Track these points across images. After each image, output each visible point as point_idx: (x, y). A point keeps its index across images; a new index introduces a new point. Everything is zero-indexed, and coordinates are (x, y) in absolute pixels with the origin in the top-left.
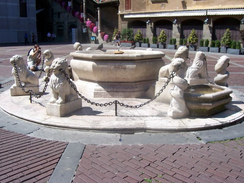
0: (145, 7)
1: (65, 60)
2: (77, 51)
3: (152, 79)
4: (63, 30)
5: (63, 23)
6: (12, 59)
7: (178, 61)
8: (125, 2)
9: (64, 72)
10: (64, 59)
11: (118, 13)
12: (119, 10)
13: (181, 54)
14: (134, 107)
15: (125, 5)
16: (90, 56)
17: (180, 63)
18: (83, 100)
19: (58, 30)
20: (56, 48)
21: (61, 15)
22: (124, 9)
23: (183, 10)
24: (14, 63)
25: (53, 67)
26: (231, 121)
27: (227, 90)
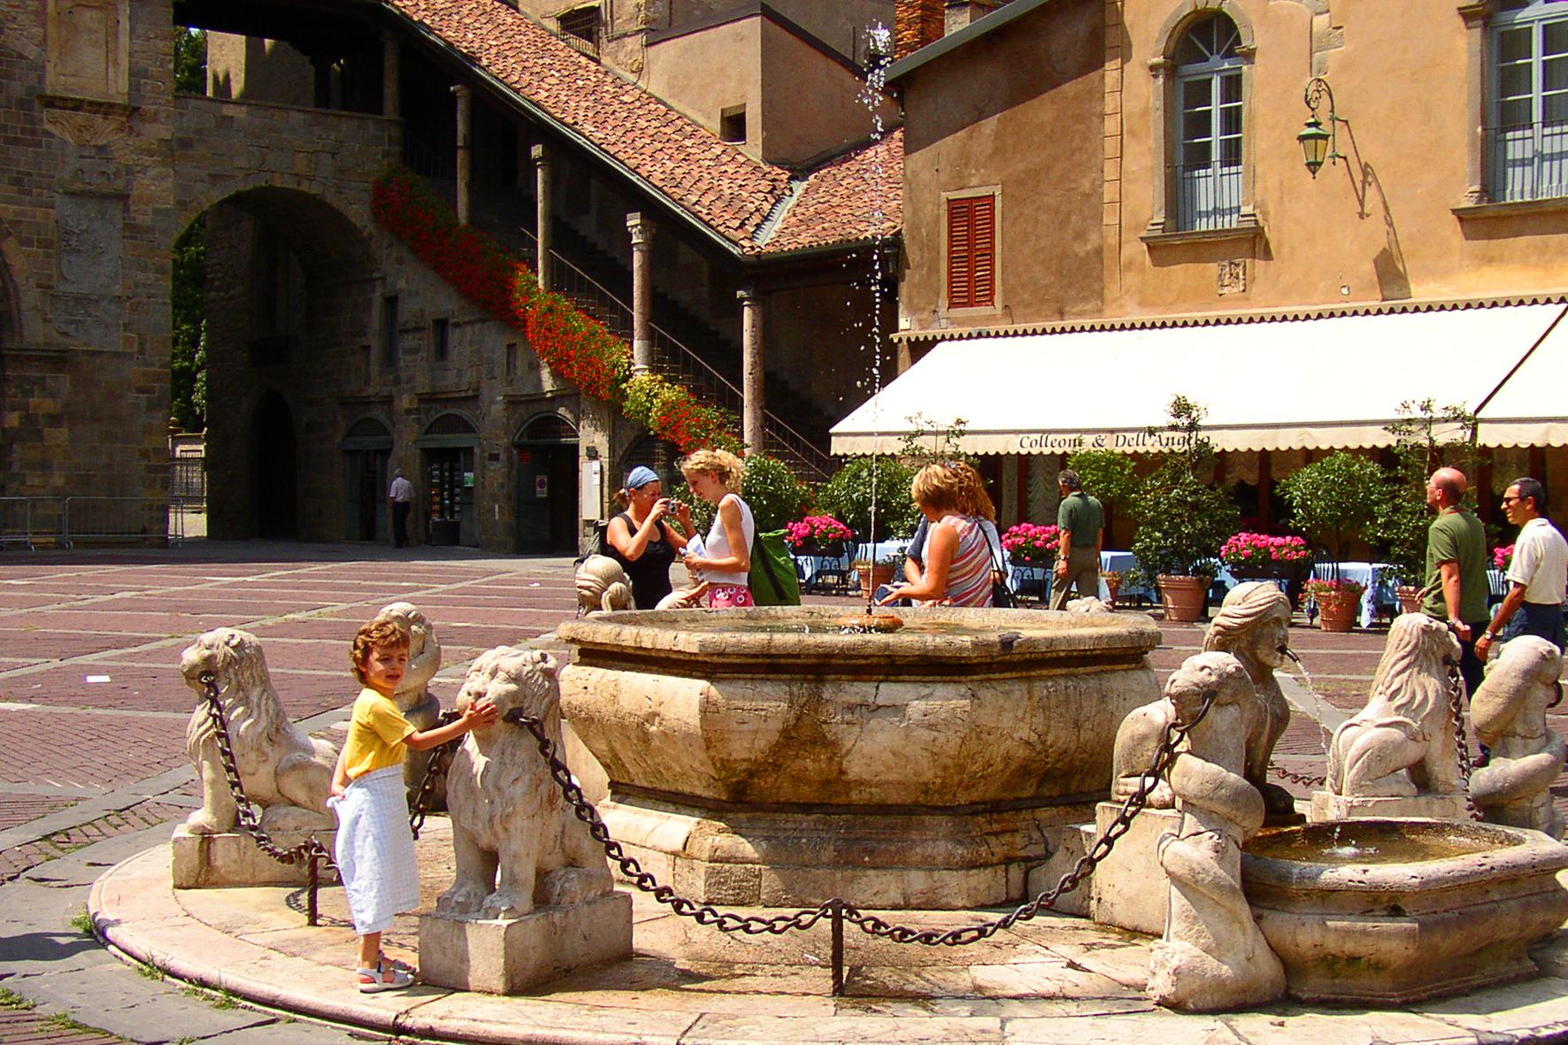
0: (1096, 286)
1: (544, 658)
2: (595, 614)
3: (1072, 782)
4: (470, 450)
5: (475, 399)
6: (192, 656)
7: (1203, 669)
8: (950, 252)
9: (537, 727)
10: (537, 655)
11: (896, 330)
12: (901, 308)
13: (1242, 626)
14: (943, 940)
15: (950, 273)
16: (687, 641)
17: (1214, 678)
18: (644, 903)
19: (433, 456)
20: (48, 609)
21: (454, 337)
22: (943, 302)
23: (1374, 304)
24: (207, 677)
25: (471, 699)
26: (1545, 1033)
27: (1536, 845)
